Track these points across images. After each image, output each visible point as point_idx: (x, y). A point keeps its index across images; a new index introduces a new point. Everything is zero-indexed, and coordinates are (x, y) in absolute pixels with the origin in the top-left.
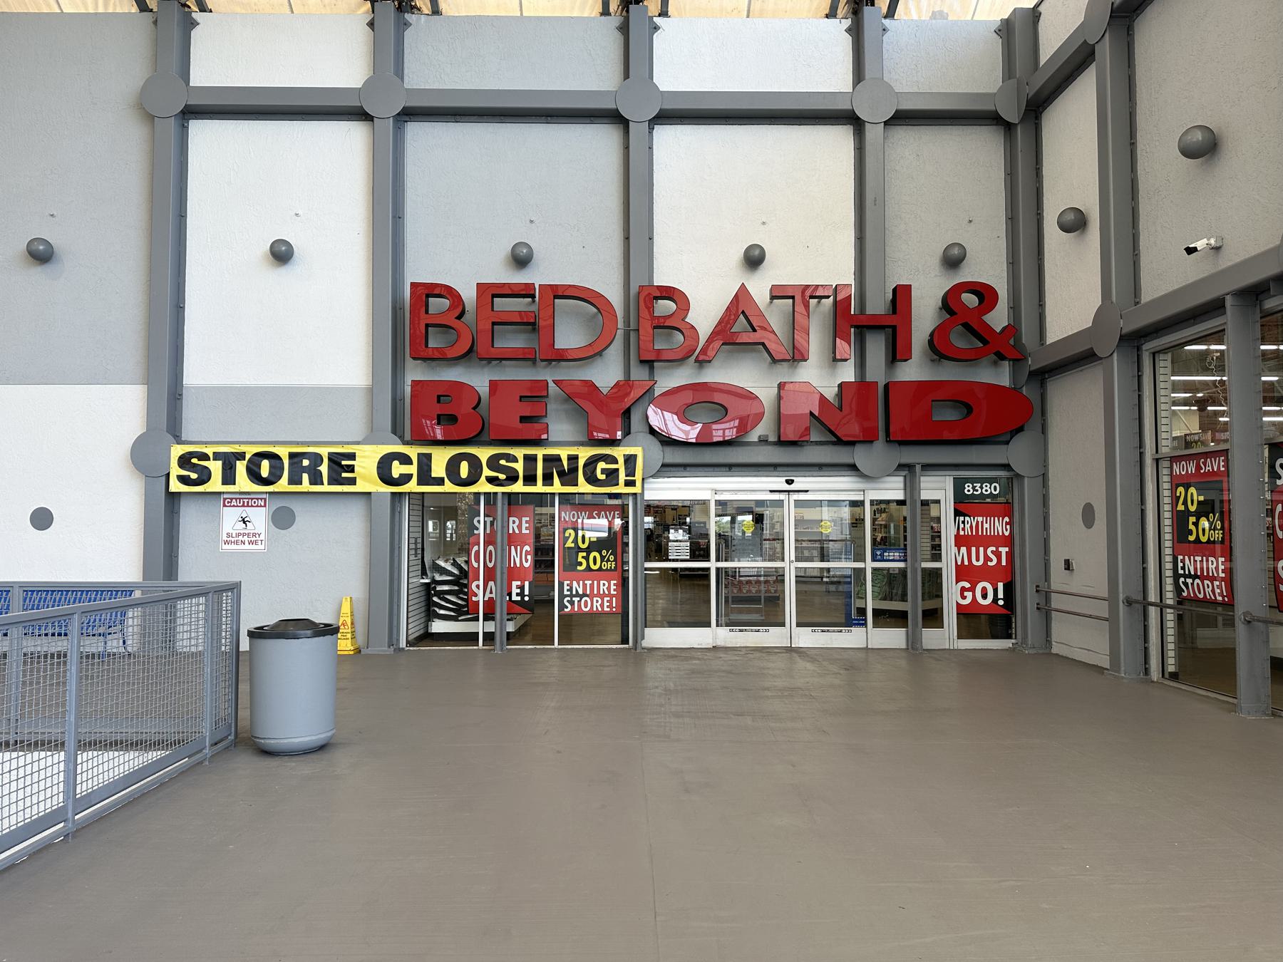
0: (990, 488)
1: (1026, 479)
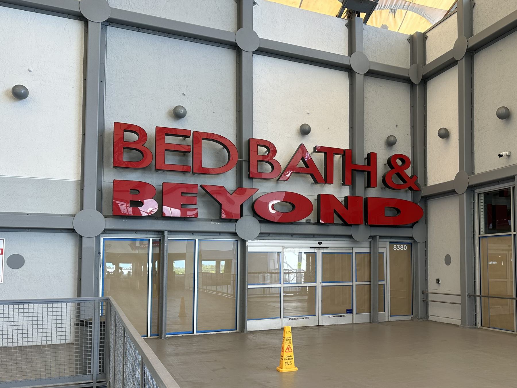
0: (403, 247)
1: (419, 244)
